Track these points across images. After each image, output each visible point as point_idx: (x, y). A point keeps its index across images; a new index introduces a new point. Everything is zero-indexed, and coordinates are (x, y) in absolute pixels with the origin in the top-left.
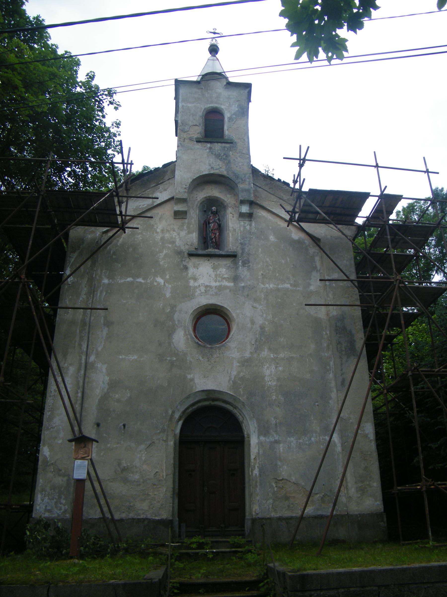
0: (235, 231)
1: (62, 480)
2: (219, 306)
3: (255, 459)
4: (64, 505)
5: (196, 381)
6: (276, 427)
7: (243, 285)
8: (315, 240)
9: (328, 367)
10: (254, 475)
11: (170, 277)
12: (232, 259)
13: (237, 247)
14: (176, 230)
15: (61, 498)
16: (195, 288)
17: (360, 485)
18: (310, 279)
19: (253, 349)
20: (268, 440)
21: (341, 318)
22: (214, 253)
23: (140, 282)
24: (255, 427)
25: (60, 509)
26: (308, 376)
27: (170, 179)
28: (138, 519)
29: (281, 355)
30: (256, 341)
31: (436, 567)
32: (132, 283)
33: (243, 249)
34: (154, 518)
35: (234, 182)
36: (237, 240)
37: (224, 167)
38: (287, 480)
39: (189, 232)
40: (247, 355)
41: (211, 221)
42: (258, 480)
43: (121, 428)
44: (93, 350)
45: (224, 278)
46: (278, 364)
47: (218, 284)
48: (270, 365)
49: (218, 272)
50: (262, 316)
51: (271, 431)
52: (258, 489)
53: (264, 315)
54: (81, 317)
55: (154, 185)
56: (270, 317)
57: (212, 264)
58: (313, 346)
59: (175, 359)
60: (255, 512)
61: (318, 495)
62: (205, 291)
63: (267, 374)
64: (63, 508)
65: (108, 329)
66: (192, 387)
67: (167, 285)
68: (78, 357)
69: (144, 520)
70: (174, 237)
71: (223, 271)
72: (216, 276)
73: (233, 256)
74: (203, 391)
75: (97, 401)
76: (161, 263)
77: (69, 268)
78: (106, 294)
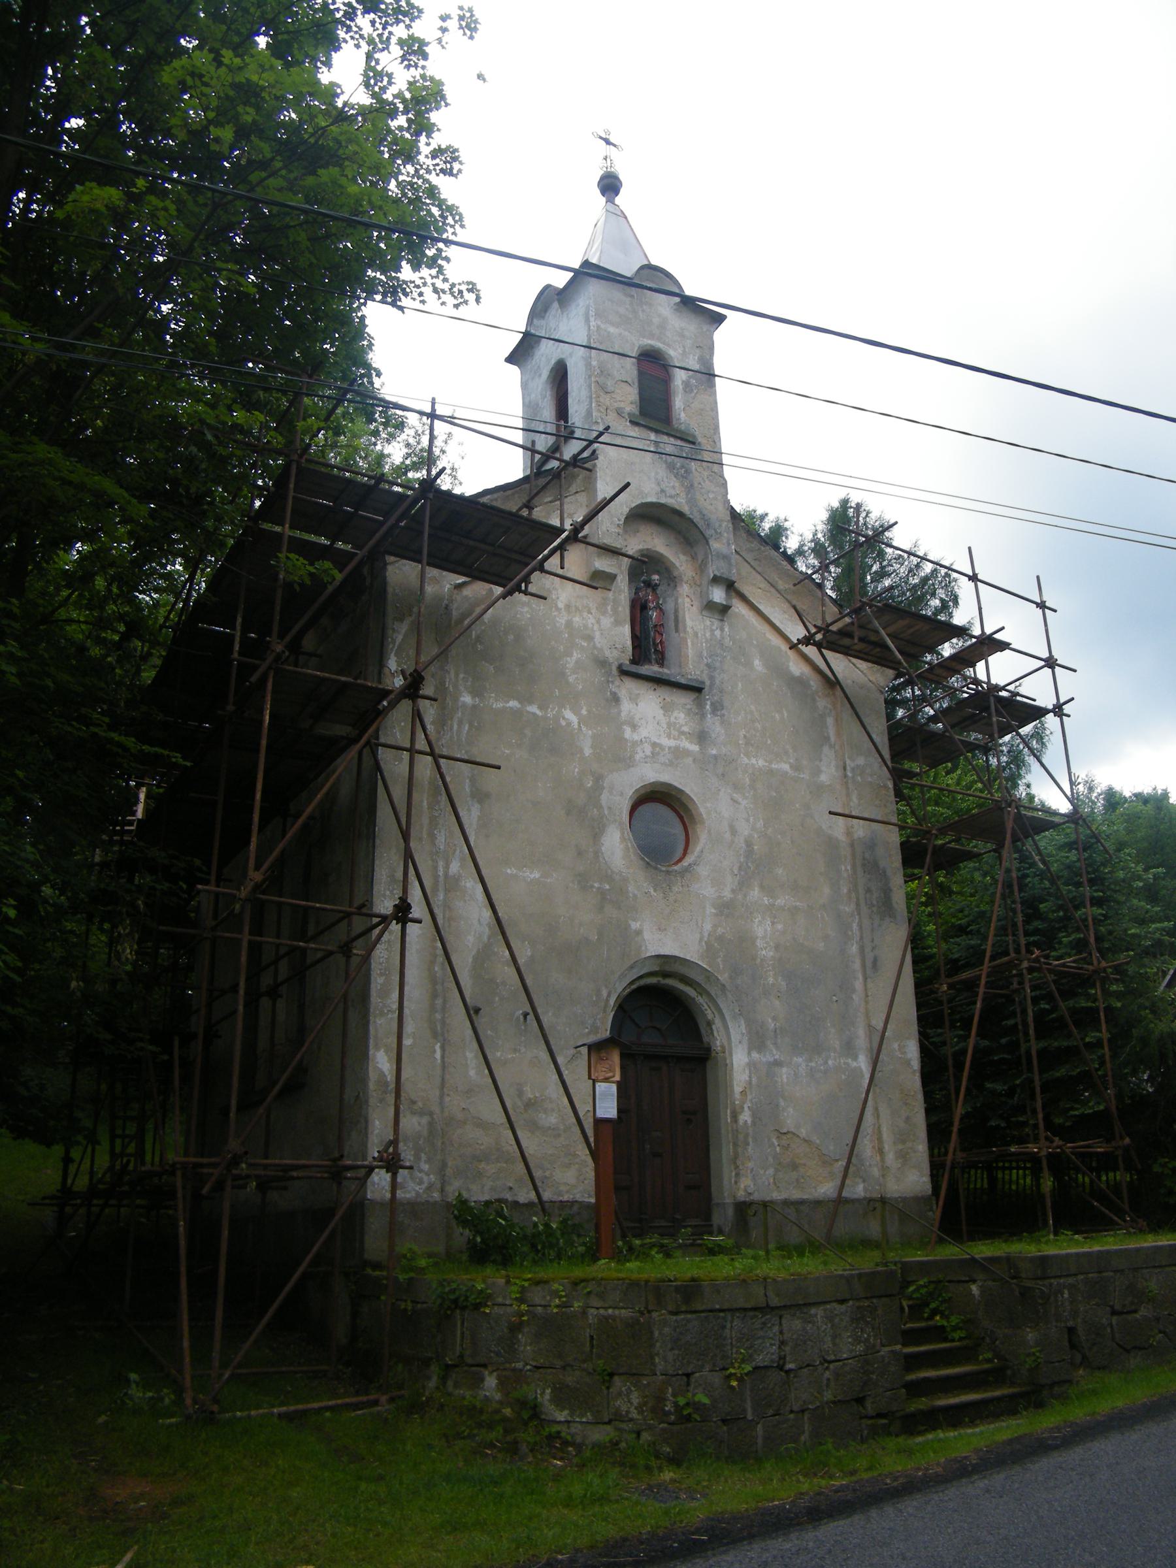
0: (697, 637)
1: (419, 1124)
2: (676, 788)
3: (743, 1093)
4: (428, 1174)
5: (647, 935)
6: (776, 1037)
7: (714, 752)
8: (832, 683)
9: (850, 933)
10: (741, 1122)
11: (589, 711)
12: (693, 695)
13: (702, 672)
14: (593, 611)
15: (420, 1159)
16: (635, 744)
17: (900, 1147)
18: (821, 761)
19: (736, 883)
20: (764, 1060)
21: (871, 845)
22: (667, 678)
23: (534, 714)
24: (743, 1034)
25: (421, 1182)
26: (821, 946)
27: (577, 492)
28: (561, 1201)
29: (780, 902)
30: (740, 868)
31: (1166, 1246)
32: (517, 714)
33: (712, 678)
34: (586, 1200)
35: (702, 533)
36: (700, 656)
37: (683, 495)
38: (794, 1134)
39: (617, 623)
40: (727, 894)
41: (651, 605)
42: (750, 1131)
43: (518, 1018)
44: (455, 850)
45: (683, 733)
46: (775, 918)
47: (672, 743)
48: (763, 918)
49: (672, 719)
50: (748, 820)
51: (769, 1043)
52: (750, 1149)
53: (751, 819)
54: (428, 772)
55: (549, 499)
56: (760, 824)
57: (661, 699)
58: (827, 890)
59: (607, 887)
60: (745, 1190)
61: (840, 1163)
62: (652, 753)
63: (760, 935)
64: (425, 1178)
65: (479, 806)
66: (641, 947)
67: (584, 729)
68: (430, 862)
69: (573, 1202)
70: (590, 625)
71: (680, 716)
72: (669, 725)
73: (695, 689)
74: (658, 956)
75: (470, 960)
76: (571, 679)
77: (392, 655)
78: (470, 729)
